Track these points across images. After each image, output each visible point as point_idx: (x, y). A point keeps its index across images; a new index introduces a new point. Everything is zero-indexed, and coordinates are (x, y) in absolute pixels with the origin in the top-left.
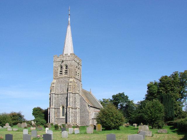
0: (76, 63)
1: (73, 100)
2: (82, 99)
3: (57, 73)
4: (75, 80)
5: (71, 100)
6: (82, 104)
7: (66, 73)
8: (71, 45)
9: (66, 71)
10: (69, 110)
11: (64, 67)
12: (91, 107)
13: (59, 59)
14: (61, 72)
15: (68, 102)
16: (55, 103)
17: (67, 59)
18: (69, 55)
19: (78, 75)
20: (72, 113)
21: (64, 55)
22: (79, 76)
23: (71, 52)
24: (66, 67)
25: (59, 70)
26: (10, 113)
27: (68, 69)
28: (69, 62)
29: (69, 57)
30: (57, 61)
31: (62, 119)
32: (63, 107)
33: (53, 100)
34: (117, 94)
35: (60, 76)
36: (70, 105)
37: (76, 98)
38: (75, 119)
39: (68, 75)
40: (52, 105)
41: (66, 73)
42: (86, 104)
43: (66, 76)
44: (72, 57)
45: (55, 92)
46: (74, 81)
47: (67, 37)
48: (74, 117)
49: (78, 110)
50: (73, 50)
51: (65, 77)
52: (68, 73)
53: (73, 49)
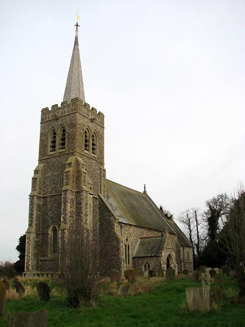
3: (47, 146)
30: (47, 120)
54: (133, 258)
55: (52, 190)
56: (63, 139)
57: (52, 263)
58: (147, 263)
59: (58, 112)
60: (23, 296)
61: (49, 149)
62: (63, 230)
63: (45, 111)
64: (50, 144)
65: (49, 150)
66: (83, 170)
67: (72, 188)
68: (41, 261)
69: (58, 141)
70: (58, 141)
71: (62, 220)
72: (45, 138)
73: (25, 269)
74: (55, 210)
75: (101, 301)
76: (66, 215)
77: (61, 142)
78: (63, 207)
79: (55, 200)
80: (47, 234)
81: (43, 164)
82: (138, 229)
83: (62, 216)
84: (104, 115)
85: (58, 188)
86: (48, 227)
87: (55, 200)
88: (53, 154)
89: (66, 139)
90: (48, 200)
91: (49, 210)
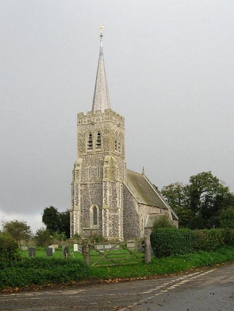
3: (85, 145)
14: (99, 143)
22: (121, 149)
25: (87, 139)
30: (83, 123)
33: (77, 194)
39: (102, 148)
46: (111, 159)
52: (102, 144)
54: (145, 228)
55: (91, 179)
56: (99, 141)
59: (94, 119)
61: (87, 147)
62: (105, 210)
63: (192, 177)
64: (87, 143)
66: (117, 166)
67: (110, 179)
69: (95, 142)
70: (95, 142)
71: (104, 202)
72: (82, 138)
73: (71, 237)
76: (106, 199)
77: (97, 143)
78: (104, 193)
80: (88, 211)
82: (148, 207)
83: (104, 199)
84: (207, 171)
86: (89, 206)
88: (91, 152)
89: (102, 141)
90: (88, 186)
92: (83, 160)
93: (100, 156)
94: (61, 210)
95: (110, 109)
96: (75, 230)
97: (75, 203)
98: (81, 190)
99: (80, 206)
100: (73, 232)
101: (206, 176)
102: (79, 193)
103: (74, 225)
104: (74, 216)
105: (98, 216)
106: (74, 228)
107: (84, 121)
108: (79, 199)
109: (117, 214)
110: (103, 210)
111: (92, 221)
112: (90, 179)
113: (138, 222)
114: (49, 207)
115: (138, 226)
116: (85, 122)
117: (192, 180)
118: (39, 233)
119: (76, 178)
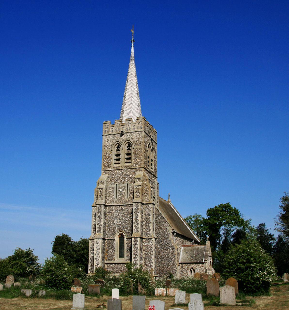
0: (148, 138)
1: (144, 220)
2: (158, 216)
3: (110, 158)
4: (147, 175)
5: (139, 218)
6: (158, 230)
7: (128, 159)
8: (136, 90)
9: (127, 154)
10: (136, 244)
11: (124, 147)
12: (178, 235)
13: (114, 129)
14: (118, 158)
15: (134, 225)
16: (104, 227)
17: (130, 129)
18: (134, 120)
19: (152, 164)
20: (141, 249)
21: (124, 121)
22: (153, 167)
23: (138, 116)
24: (129, 146)
25: (115, 152)
26: (14, 254)
27: (133, 150)
28: (134, 135)
29: (134, 124)
30: (110, 133)
31: (119, 264)
32: (122, 238)
33: (100, 218)
34: (216, 207)
35: (115, 166)
36: (138, 231)
37: (149, 215)
38: (147, 264)
39: (133, 162)
40: (98, 231)
41: (128, 159)
42: (168, 228)
43: (128, 166)
44: (140, 125)
45: (106, 202)
46: (144, 175)
47: (129, 78)
48: (145, 259)
49: (153, 243)
50: (141, 113)
51: (127, 168)
52: (133, 158)
53: (140, 109)
55: (118, 200)
57: (119, 266)
58: (192, 268)
60: (42, 266)
64: (114, 157)
65: (113, 163)
68: (106, 264)
69: (123, 156)
70: (123, 156)
73: (89, 272)
74: (122, 219)
75: (47, 259)
76: (138, 224)
79: (122, 209)
81: (107, 175)
84: (25, 248)
85: (125, 199)
87: (122, 209)
89: (133, 155)
91: (115, 218)
92: (108, 177)
93: (130, 172)
94: (76, 238)
95: (131, 118)
96: (95, 264)
97: (97, 229)
98: (105, 213)
99: (102, 233)
100: (92, 266)
101: (28, 254)
102: (102, 217)
103: (95, 257)
104: (95, 246)
105: (126, 246)
106: (95, 260)
107: (111, 130)
108: (102, 224)
109: (150, 245)
110: (133, 239)
111: (117, 252)
112: (116, 200)
113: (174, 257)
114: (61, 235)
115: (174, 261)
116: (112, 132)
117: (210, 212)
118: (49, 264)
119: (99, 198)
